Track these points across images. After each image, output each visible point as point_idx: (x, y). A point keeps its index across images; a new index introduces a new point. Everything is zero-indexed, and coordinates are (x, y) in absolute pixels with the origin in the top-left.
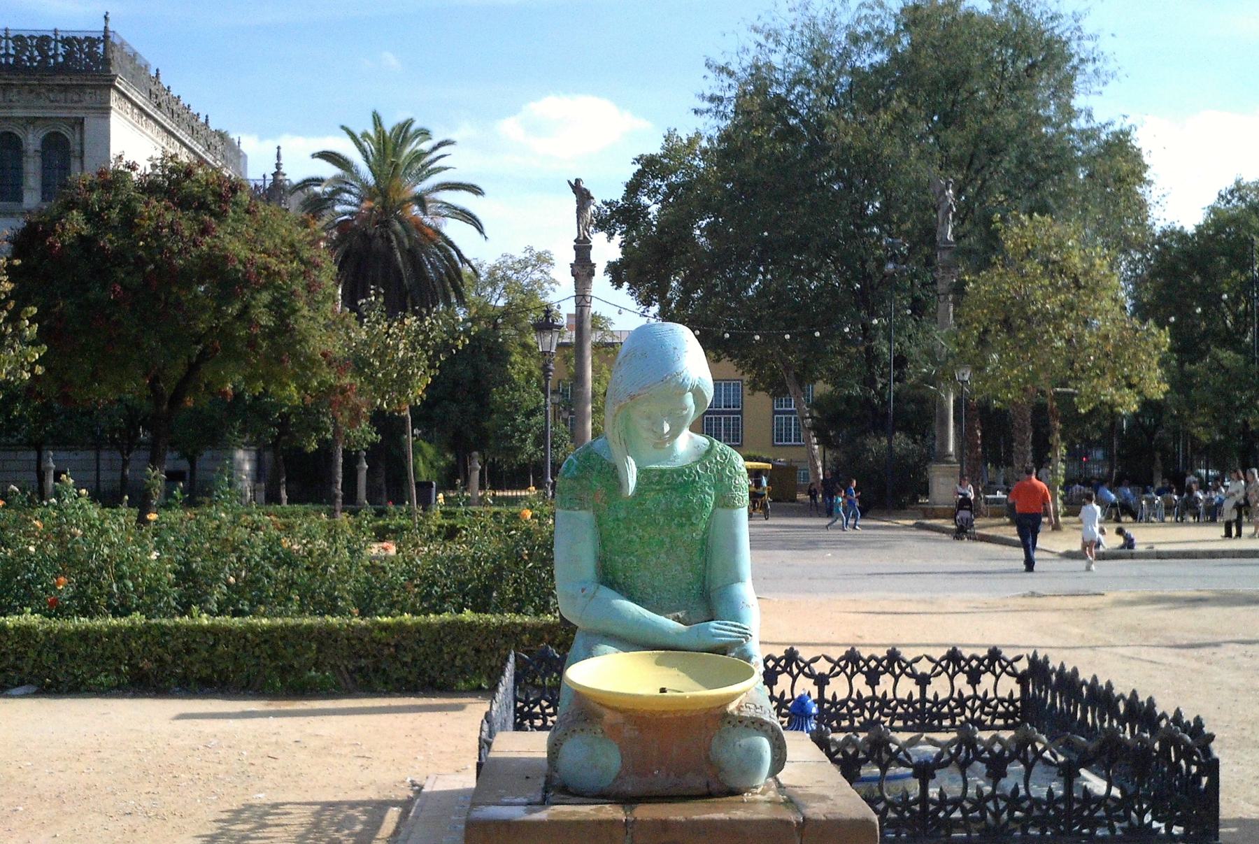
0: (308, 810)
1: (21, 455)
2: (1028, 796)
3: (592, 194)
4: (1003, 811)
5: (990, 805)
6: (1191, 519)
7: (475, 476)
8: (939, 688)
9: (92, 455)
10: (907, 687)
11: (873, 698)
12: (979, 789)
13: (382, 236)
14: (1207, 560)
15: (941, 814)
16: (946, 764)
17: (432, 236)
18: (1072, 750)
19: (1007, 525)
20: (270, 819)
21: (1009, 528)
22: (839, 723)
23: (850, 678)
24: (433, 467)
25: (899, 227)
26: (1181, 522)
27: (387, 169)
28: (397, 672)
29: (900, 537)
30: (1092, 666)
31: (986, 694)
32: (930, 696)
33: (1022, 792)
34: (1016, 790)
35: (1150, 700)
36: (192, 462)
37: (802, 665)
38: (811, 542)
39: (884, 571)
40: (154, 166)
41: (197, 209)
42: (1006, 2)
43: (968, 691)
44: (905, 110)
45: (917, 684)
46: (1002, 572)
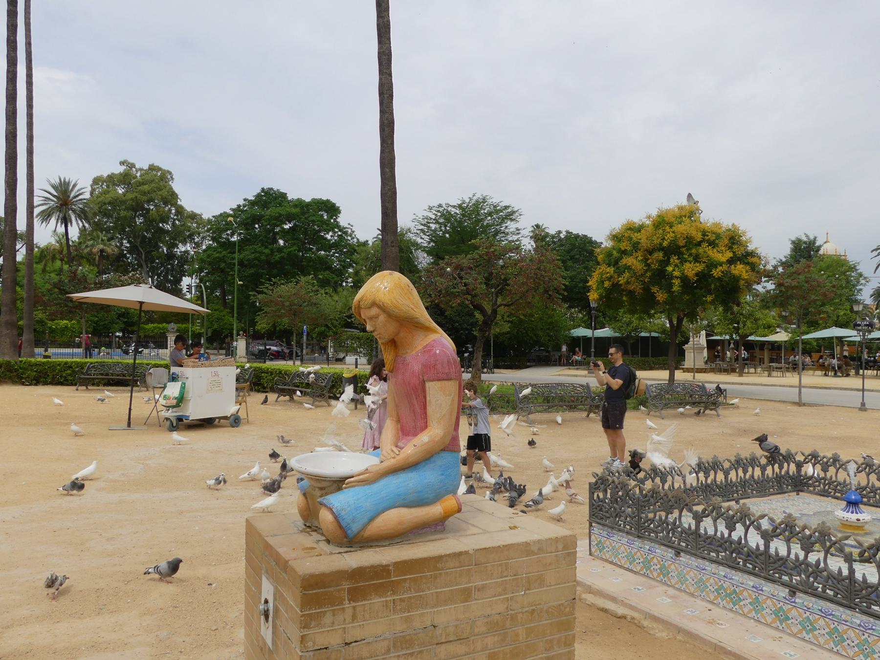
0: (596, 529)
3: (300, 189)
6: (453, 211)
7: (593, 354)
8: (778, 546)
10: (836, 564)
11: (824, 479)
12: (797, 556)
13: (313, 338)
16: (807, 463)
17: (271, 211)
19: (590, 590)
20: (439, 565)
21: (589, 581)
23: (868, 475)
28: (60, 340)
30: (419, 298)
31: (831, 477)
35: (245, 200)
39: (777, 405)
41: (316, 270)
42: (878, 484)
43: (822, 475)
44: (121, 256)
46: (823, 405)
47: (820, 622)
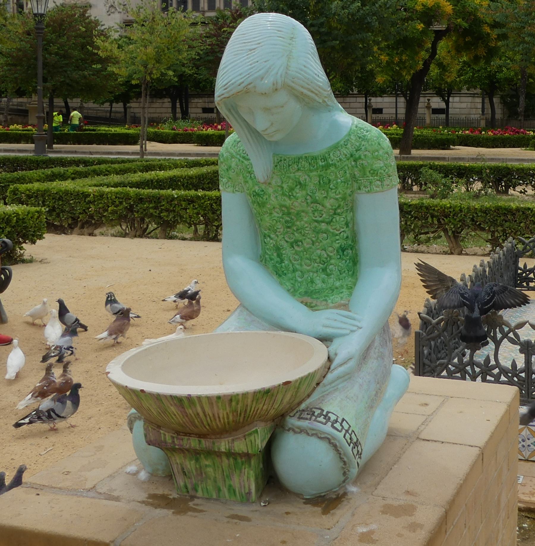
1: (359, 100)
2: (498, 365)
4: (126, 229)
5: (468, 368)
9: (393, 99)
14: (160, 151)
15: (524, 275)
18: (180, 449)
22: (528, 284)
24: (350, 135)
25: (316, 418)
26: (189, 398)
27: (360, 366)
29: (309, 90)
32: (517, 246)
33: (493, 362)
34: (488, 360)
36: (447, 103)
37: (506, 329)
38: (302, 87)
40: (74, 191)
45: (521, 351)
47: (523, 433)
